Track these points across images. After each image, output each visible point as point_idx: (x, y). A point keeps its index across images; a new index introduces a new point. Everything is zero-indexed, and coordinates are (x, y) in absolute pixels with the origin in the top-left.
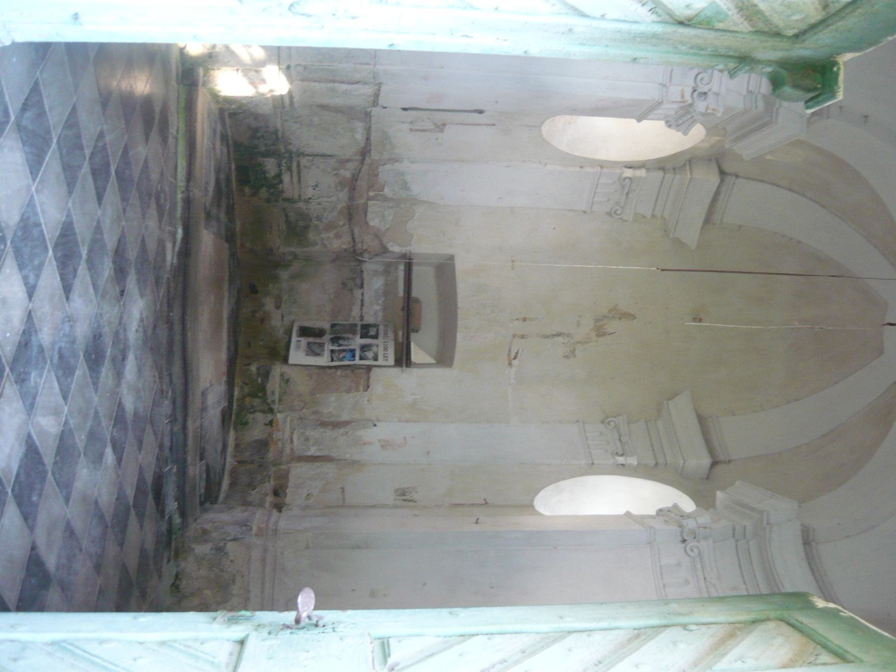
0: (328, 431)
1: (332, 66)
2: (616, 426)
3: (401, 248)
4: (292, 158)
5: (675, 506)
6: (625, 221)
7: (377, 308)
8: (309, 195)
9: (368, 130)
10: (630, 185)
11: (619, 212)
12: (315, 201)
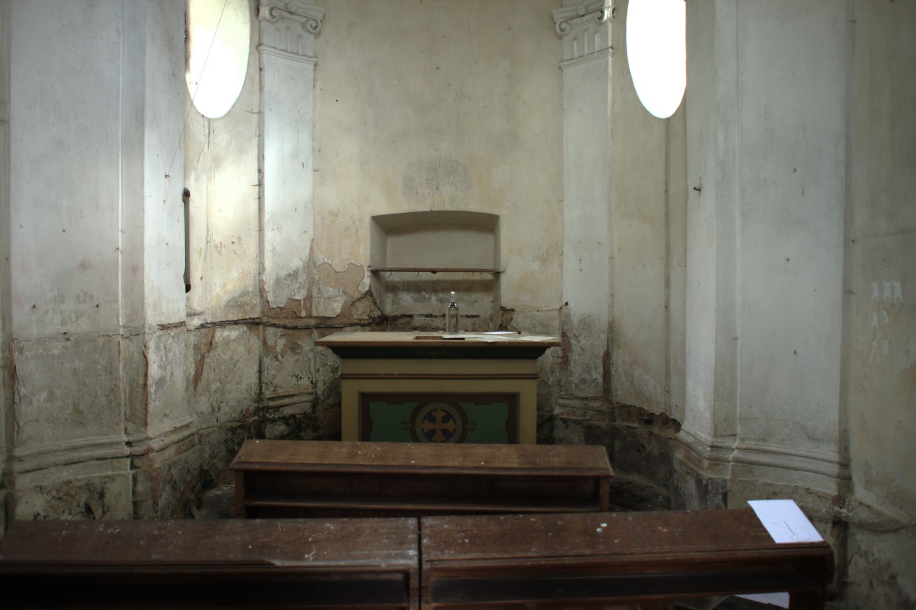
0: (574, 358)
1: (125, 389)
2: (566, 21)
3: (366, 277)
4: (264, 408)
6: (324, 16)
7: (434, 298)
8: (308, 383)
9: (223, 324)
10: (280, 9)
11: (314, 24)
12: (314, 376)
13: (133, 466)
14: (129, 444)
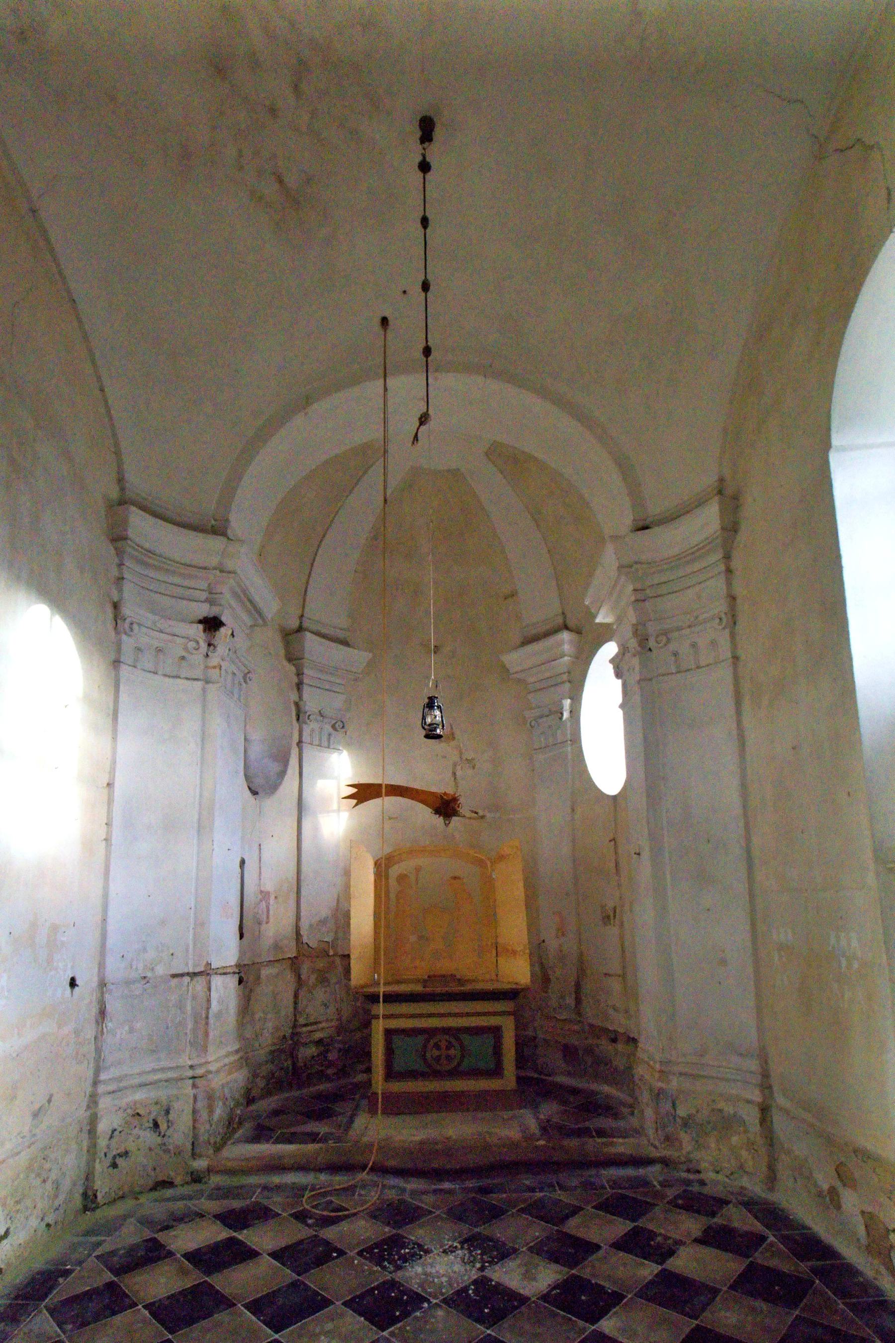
5: (612, 661)
13: (194, 1086)
14: (191, 1067)
